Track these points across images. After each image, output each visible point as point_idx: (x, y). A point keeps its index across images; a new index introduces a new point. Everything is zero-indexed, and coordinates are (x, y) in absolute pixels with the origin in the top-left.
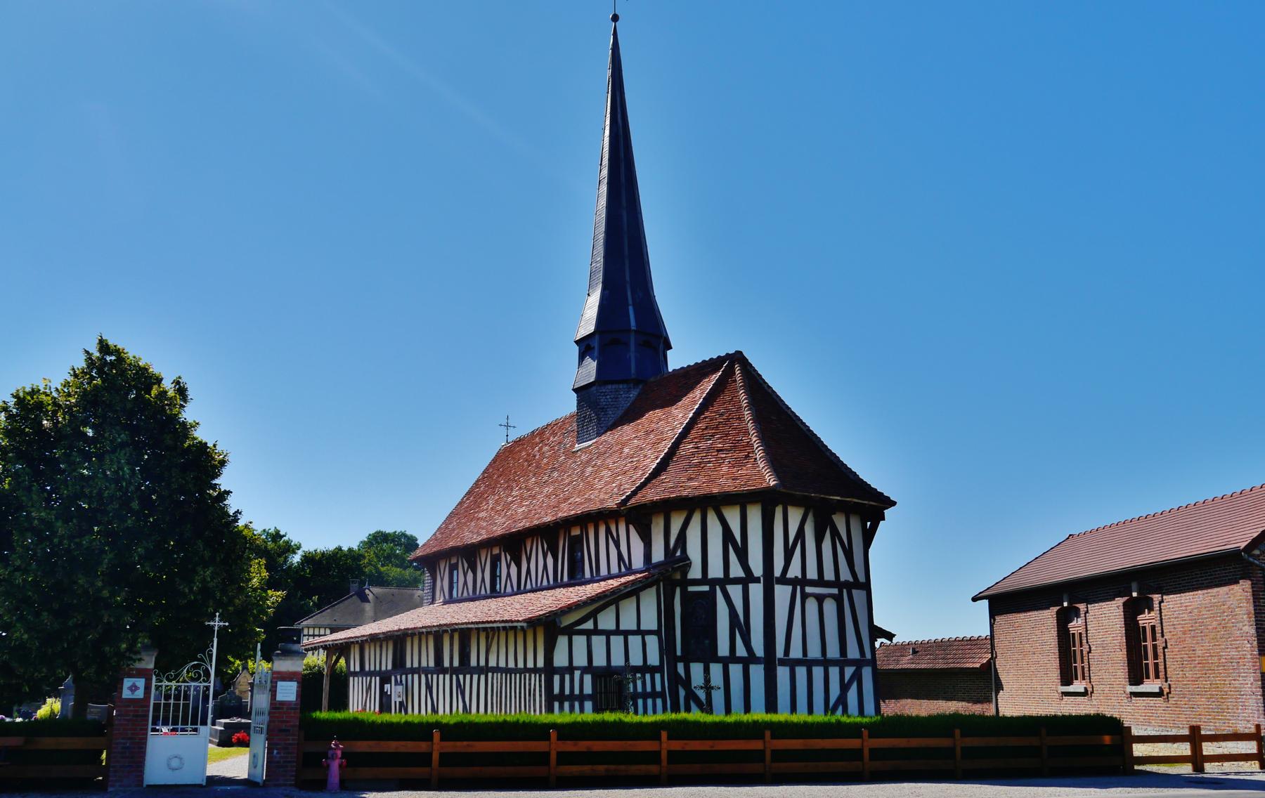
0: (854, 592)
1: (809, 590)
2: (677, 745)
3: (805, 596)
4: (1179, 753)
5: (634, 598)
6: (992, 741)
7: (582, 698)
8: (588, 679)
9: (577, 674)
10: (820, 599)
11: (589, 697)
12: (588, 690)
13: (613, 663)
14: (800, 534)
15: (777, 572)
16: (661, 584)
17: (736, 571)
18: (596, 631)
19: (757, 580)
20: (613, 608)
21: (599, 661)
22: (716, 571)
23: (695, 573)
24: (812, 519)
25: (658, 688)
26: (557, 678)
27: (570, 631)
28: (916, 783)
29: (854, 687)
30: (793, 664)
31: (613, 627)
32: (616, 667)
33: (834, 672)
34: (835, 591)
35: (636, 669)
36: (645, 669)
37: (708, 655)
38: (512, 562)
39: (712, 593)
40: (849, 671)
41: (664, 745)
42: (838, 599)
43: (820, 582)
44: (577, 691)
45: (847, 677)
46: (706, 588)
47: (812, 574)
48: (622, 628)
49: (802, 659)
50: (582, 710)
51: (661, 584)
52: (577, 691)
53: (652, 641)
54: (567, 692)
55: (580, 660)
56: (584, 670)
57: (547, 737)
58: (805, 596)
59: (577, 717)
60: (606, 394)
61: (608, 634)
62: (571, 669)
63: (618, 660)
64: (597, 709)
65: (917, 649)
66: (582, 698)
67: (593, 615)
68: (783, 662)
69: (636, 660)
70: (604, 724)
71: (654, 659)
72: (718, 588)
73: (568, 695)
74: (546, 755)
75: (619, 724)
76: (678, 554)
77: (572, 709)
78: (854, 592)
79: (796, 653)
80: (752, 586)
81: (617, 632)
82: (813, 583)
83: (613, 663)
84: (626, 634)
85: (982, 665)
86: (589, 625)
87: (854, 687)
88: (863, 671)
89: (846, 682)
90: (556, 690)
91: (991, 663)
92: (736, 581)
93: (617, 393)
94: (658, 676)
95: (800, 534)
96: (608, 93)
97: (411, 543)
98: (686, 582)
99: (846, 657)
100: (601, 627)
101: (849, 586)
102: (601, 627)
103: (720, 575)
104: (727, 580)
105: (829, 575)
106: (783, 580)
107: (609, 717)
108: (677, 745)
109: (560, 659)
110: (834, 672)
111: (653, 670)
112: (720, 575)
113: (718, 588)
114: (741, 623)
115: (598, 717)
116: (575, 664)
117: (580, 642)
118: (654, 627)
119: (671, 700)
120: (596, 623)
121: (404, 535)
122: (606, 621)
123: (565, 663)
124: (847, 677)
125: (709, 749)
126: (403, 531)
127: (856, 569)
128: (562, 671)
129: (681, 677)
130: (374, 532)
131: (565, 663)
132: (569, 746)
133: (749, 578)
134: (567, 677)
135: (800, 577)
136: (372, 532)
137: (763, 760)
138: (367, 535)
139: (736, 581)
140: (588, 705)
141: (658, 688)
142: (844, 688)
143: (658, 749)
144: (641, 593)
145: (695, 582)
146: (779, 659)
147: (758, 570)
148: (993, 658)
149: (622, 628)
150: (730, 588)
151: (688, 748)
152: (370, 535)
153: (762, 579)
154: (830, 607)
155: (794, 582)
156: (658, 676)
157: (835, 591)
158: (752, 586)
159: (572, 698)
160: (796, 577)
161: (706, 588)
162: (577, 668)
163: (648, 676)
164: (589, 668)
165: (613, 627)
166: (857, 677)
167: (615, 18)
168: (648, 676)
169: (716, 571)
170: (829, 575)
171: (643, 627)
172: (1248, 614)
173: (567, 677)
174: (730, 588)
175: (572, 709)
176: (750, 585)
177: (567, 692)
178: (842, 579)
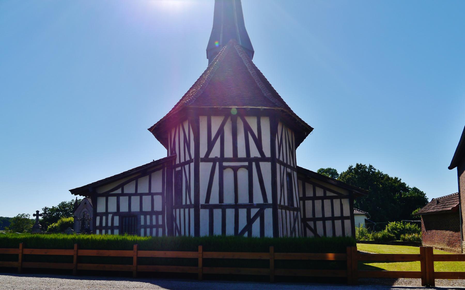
0: (262, 164)
1: (225, 164)
2: (279, 256)
3: (222, 169)
4: (445, 281)
7: (113, 228)
8: (117, 219)
9: (110, 216)
10: (235, 170)
11: (117, 228)
12: (116, 223)
14: (221, 132)
15: (202, 154)
16: (166, 168)
18: (123, 194)
20: (134, 182)
21: (124, 208)
24: (231, 122)
25: (160, 223)
26: (98, 219)
27: (107, 195)
29: (258, 220)
30: (211, 208)
31: (133, 192)
32: (134, 212)
33: (243, 213)
34: (246, 164)
35: (146, 214)
36: (152, 213)
38: (294, 172)
40: (254, 212)
42: (249, 169)
44: (110, 224)
45: (252, 215)
47: (229, 153)
49: (204, 205)
50: (112, 233)
51: (166, 168)
52: (110, 224)
54: (104, 224)
55: (112, 208)
56: (114, 214)
58: (222, 169)
59: (110, 237)
61: (130, 195)
62: (106, 214)
63: (135, 208)
64: (121, 233)
65: (437, 201)
66: (113, 228)
67: (122, 186)
68: (204, 207)
75: (55, 240)
77: (106, 232)
78: (262, 164)
79: (214, 200)
81: (136, 194)
84: (141, 195)
85: (453, 208)
86: (119, 191)
87: (258, 220)
89: (252, 217)
91: (459, 206)
94: (160, 217)
97: (334, 172)
100: (125, 192)
101: (257, 160)
102: (125, 192)
105: (242, 154)
106: (206, 159)
108: (279, 256)
109: (101, 208)
110: (243, 213)
111: (157, 213)
114: (188, 185)
115: (120, 238)
118: (160, 190)
119: (168, 229)
120: (123, 190)
122: (130, 189)
123: (104, 211)
124: (252, 215)
125: (44, 254)
126: (330, 168)
128: (101, 215)
131: (104, 211)
132: (27, 251)
134: (104, 218)
135: (219, 156)
136: (319, 169)
137: (197, 265)
140: (116, 232)
141: (160, 223)
142: (250, 221)
144: (152, 174)
146: (202, 205)
148: (460, 204)
151: (33, 253)
152: (318, 170)
154: (243, 174)
155: (214, 160)
156: (160, 217)
157: (246, 164)
160: (216, 157)
162: (111, 213)
163: (154, 217)
164: (118, 213)
165: (133, 192)
166: (261, 214)
168: (154, 217)
170: (242, 154)
171: (152, 191)
173: (104, 218)
175: (106, 232)
177: (104, 224)
178: (252, 155)
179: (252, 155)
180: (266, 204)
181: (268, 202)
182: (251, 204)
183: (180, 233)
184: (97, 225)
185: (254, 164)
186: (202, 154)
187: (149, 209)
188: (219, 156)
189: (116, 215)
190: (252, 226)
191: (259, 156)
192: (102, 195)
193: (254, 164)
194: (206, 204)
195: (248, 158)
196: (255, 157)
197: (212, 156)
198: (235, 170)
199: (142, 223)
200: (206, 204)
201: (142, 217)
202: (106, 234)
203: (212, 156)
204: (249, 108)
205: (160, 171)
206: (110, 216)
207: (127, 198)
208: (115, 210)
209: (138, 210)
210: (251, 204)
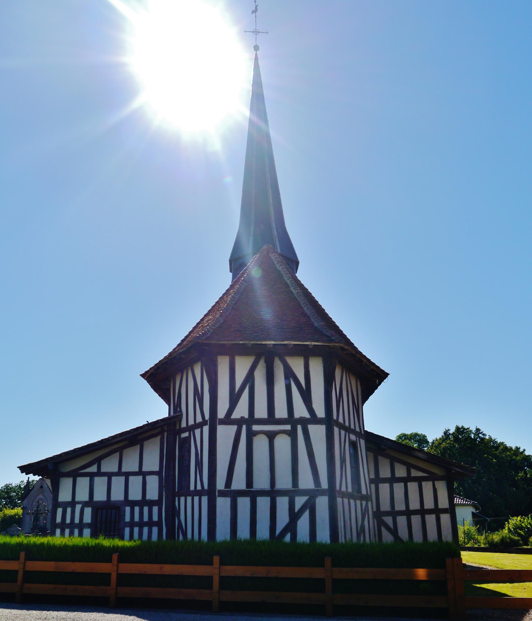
0: (311, 428)
1: (255, 428)
3: (251, 435)
5: (138, 447)
6: (260, 571)
8: (88, 511)
9: (78, 507)
10: (271, 436)
11: (88, 525)
12: (88, 518)
13: (113, 498)
14: (250, 379)
15: (221, 414)
16: (166, 434)
18: (99, 474)
20: (117, 455)
21: (100, 496)
24: (265, 365)
25: (155, 518)
26: (60, 511)
27: (75, 475)
28: (28, 609)
30: (234, 495)
31: (116, 470)
32: (115, 501)
34: (288, 427)
35: (133, 504)
36: (144, 502)
37: (185, 491)
41: (216, 571)
42: (293, 434)
43: (271, 419)
44: (77, 521)
45: (298, 507)
47: (261, 412)
48: (124, 470)
50: (81, 535)
51: (166, 434)
52: (77, 521)
53: (153, 482)
54: (68, 521)
55: (82, 495)
56: (85, 504)
57: (109, 560)
58: (251, 435)
59: (76, 541)
61: (109, 475)
62: (73, 503)
63: (118, 495)
64: (94, 535)
66: (81, 526)
67: (98, 461)
68: (223, 494)
69: (135, 495)
70: (99, 548)
71: (153, 494)
73: (68, 524)
74: (209, 579)
77: (71, 534)
78: (311, 428)
81: (119, 473)
82: (261, 422)
83: (113, 498)
84: (127, 475)
86: (93, 469)
87: (306, 515)
88: (257, 498)
90: (59, 519)
94: (155, 509)
95: (250, 379)
100: (104, 469)
101: (304, 422)
102: (104, 469)
105: (281, 412)
106: (228, 420)
107: (106, 542)
109: (65, 496)
111: (151, 504)
115: (93, 542)
116: (77, 499)
117: (83, 483)
118: (156, 468)
120: (99, 467)
121: (416, 435)
123: (69, 499)
124: (298, 507)
126: (416, 432)
127: (315, 406)
128: (65, 505)
130: (399, 434)
131: (69, 499)
134: (69, 510)
135: (246, 416)
137: (210, 587)
138: (396, 436)
140: (87, 532)
141: (155, 518)
142: (294, 516)
149: (124, 470)
155: (240, 422)
156: (155, 509)
157: (288, 427)
159: (72, 526)
162: (79, 503)
164: (90, 503)
165: (116, 470)
168: (146, 509)
170: (281, 412)
171: (144, 469)
173: (69, 510)
177: (68, 521)
178: (297, 415)
179: (297, 415)
180: (318, 489)
181: (321, 487)
182: (295, 490)
183: (185, 535)
184: (57, 522)
185: (299, 427)
186: (221, 414)
187: (139, 497)
188: (246, 416)
189: (88, 507)
190: (296, 524)
191: (307, 415)
192: (67, 475)
193: (299, 427)
194: (226, 489)
195: (291, 419)
197: (236, 415)
198: (271, 436)
199: (127, 519)
200: (226, 489)
201: (128, 509)
202: (70, 536)
203: (236, 415)
204: (291, 344)
205: (157, 438)
206: (78, 507)
207: (105, 479)
208: (86, 498)
209: (122, 498)
210: (295, 489)
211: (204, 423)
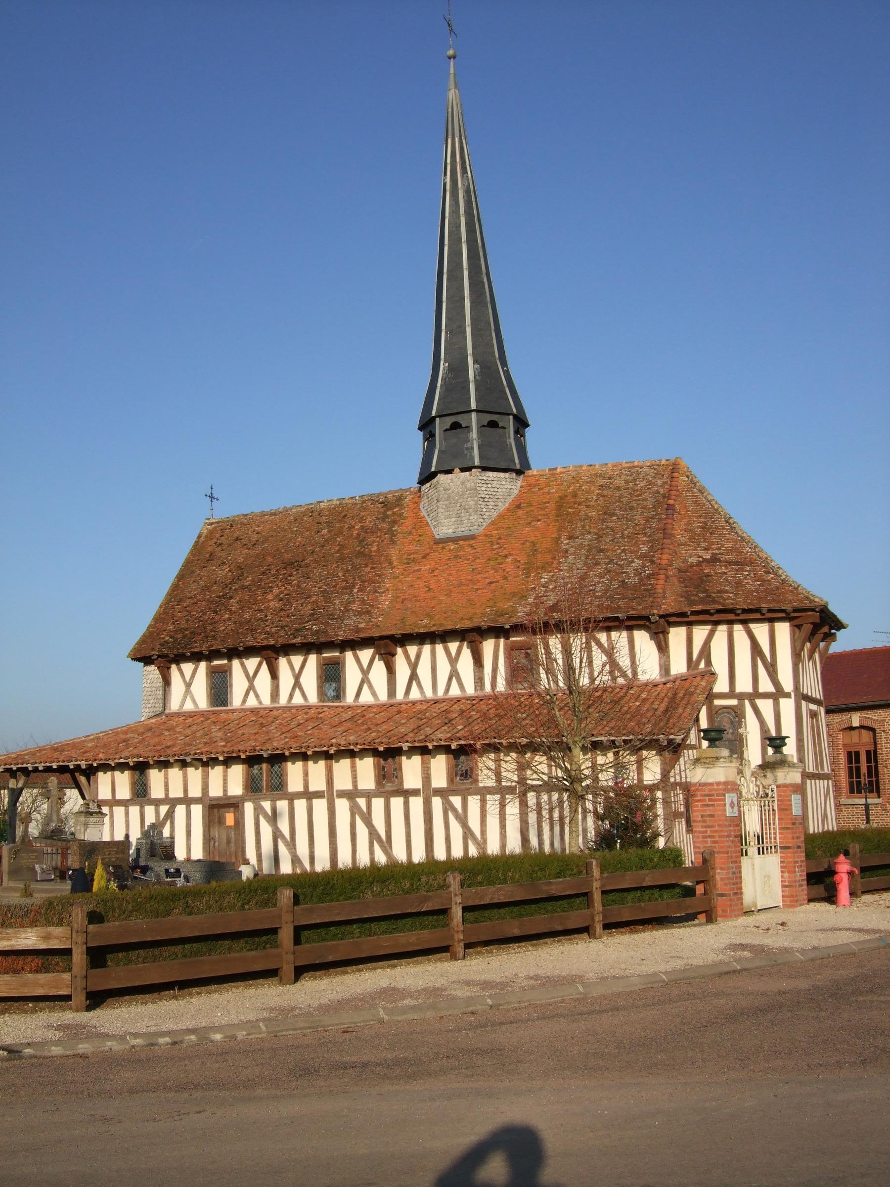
17: (766, 686)
19: (788, 695)
22: (744, 685)
23: (721, 687)
39: (741, 706)
40: (164, 809)
46: (734, 702)
49: (328, 799)
60: (487, 482)
72: (747, 703)
76: (702, 665)
80: (783, 701)
92: (766, 696)
93: (499, 482)
96: (445, 174)
98: (710, 696)
99: (434, 796)
103: (750, 689)
104: (756, 695)
107: (173, 879)
112: (750, 689)
113: (747, 703)
129: (363, 811)
133: (778, 694)
139: (766, 696)
143: (296, 947)
145: (722, 696)
147: (787, 684)
150: (760, 703)
153: (793, 694)
158: (783, 701)
161: (734, 702)
167: (449, 10)
169: (744, 685)
172: (521, 915)
174: (760, 703)
176: (780, 699)
196: (651, 639)
211: (778, 694)
